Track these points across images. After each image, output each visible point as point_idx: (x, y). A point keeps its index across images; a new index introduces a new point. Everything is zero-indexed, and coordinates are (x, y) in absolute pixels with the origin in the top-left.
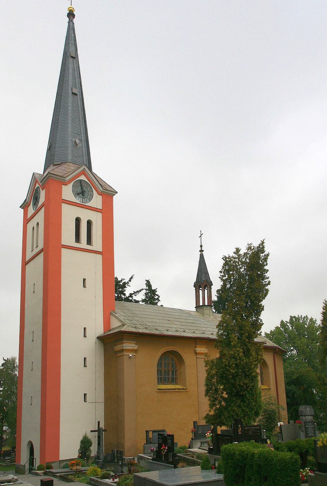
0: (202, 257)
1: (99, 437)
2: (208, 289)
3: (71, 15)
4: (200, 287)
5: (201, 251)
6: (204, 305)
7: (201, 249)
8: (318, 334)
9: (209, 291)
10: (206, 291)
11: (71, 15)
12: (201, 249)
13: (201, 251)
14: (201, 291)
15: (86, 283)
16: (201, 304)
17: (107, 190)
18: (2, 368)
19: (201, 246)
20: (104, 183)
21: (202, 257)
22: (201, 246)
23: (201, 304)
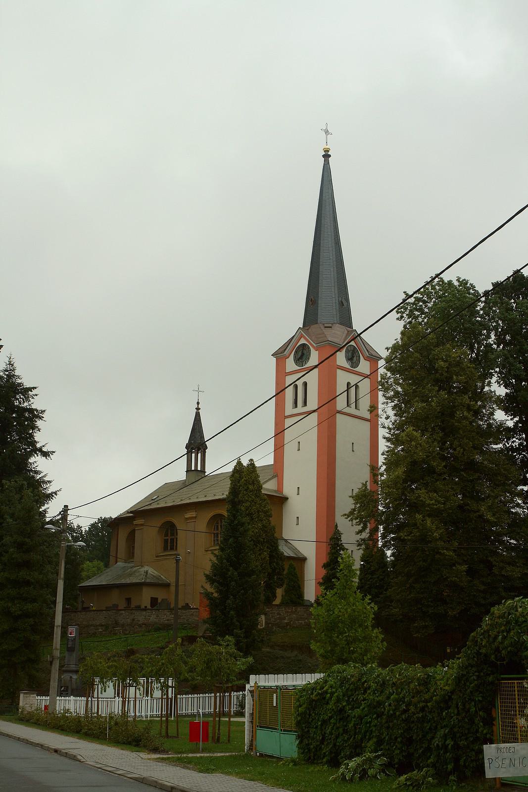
0: (198, 416)
1: (87, 704)
2: (202, 452)
3: (327, 156)
4: (192, 449)
5: (198, 409)
6: (196, 470)
7: (198, 406)
8: (520, 488)
9: (202, 454)
10: (199, 455)
11: (327, 156)
12: (198, 406)
13: (198, 409)
14: (193, 455)
15: (359, 403)
16: (193, 469)
17: (372, 355)
18: (2, 374)
19: (198, 403)
20: (375, 353)
21: (198, 416)
22: (198, 403)
23: (193, 469)
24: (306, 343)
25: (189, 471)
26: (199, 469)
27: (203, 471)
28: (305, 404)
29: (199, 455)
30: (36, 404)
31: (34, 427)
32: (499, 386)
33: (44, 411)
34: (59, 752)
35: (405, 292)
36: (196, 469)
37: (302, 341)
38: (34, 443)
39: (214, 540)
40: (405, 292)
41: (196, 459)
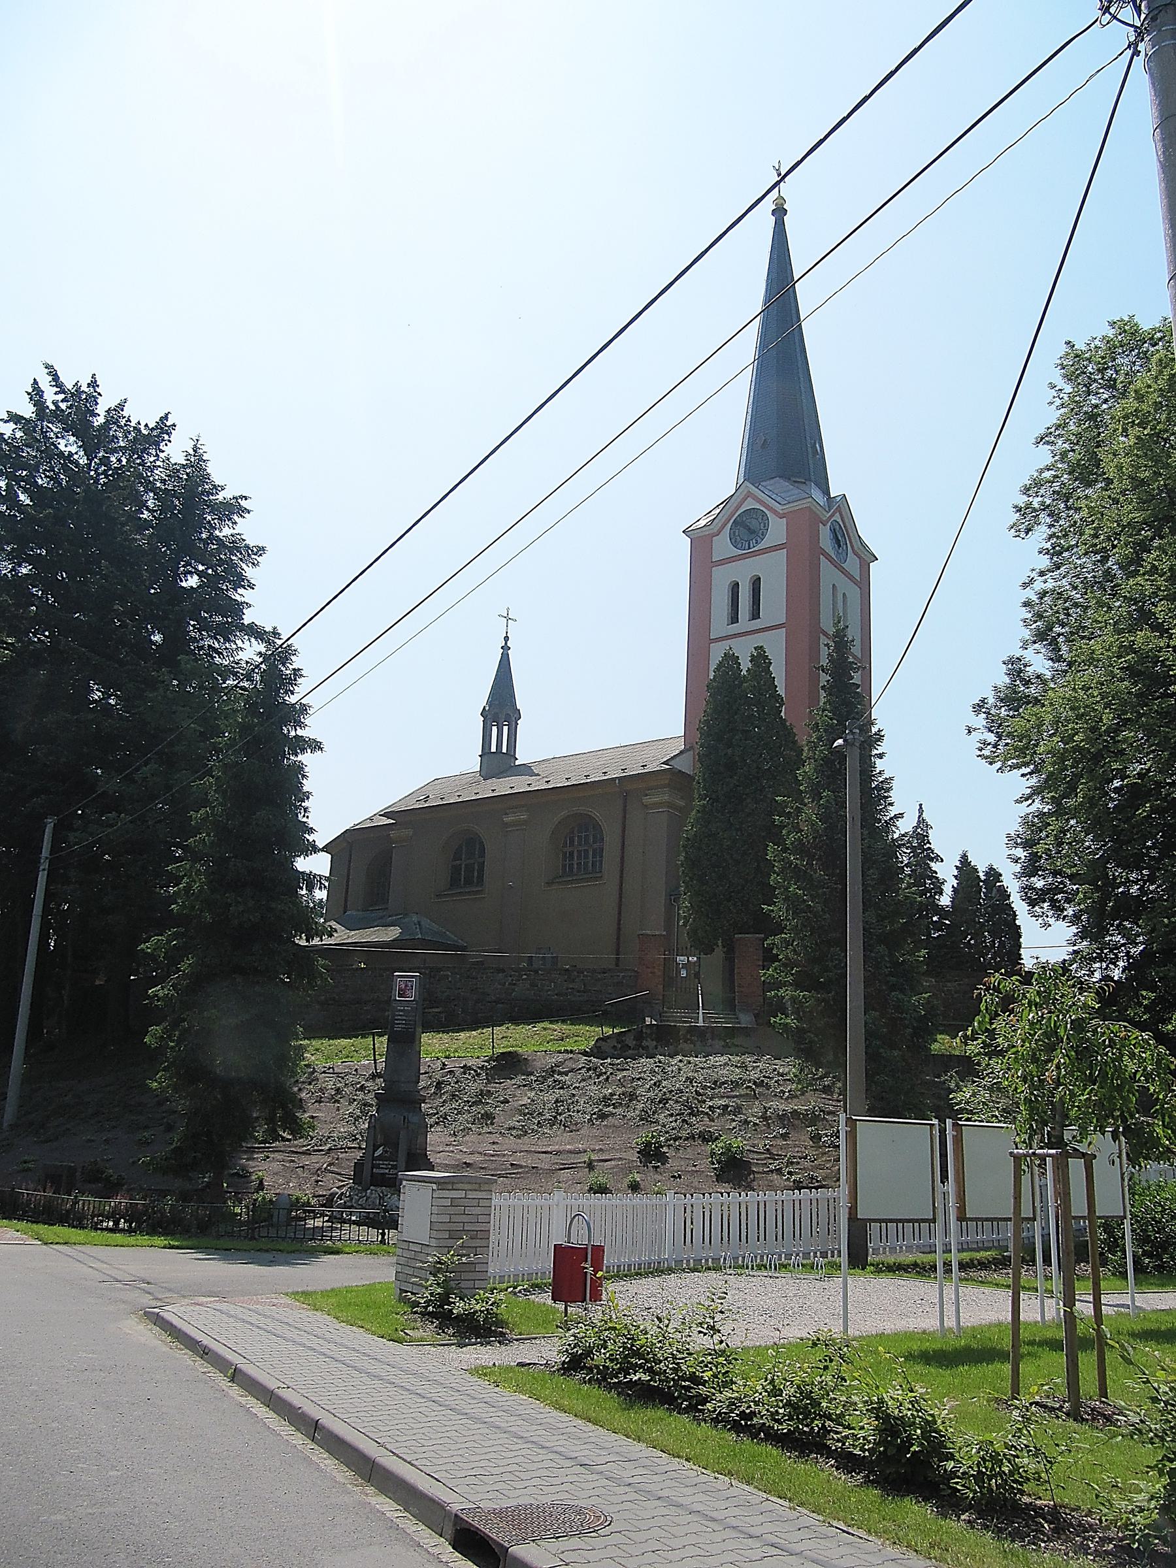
7: (506, 643)
10: (506, 729)
12: (506, 643)
16: (493, 749)
23: (493, 749)
24: (758, 506)
25: (485, 753)
26: (504, 750)
27: (511, 754)
28: (755, 615)
29: (506, 729)
30: (247, 529)
31: (240, 581)
32: (883, 736)
33: (263, 549)
34: (1046, 1231)
35: (1068, 343)
36: (499, 751)
37: (750, 504)
38: (237, 609)
39: (564, 866)
40: (1068, 343)
41: (500, 739)
